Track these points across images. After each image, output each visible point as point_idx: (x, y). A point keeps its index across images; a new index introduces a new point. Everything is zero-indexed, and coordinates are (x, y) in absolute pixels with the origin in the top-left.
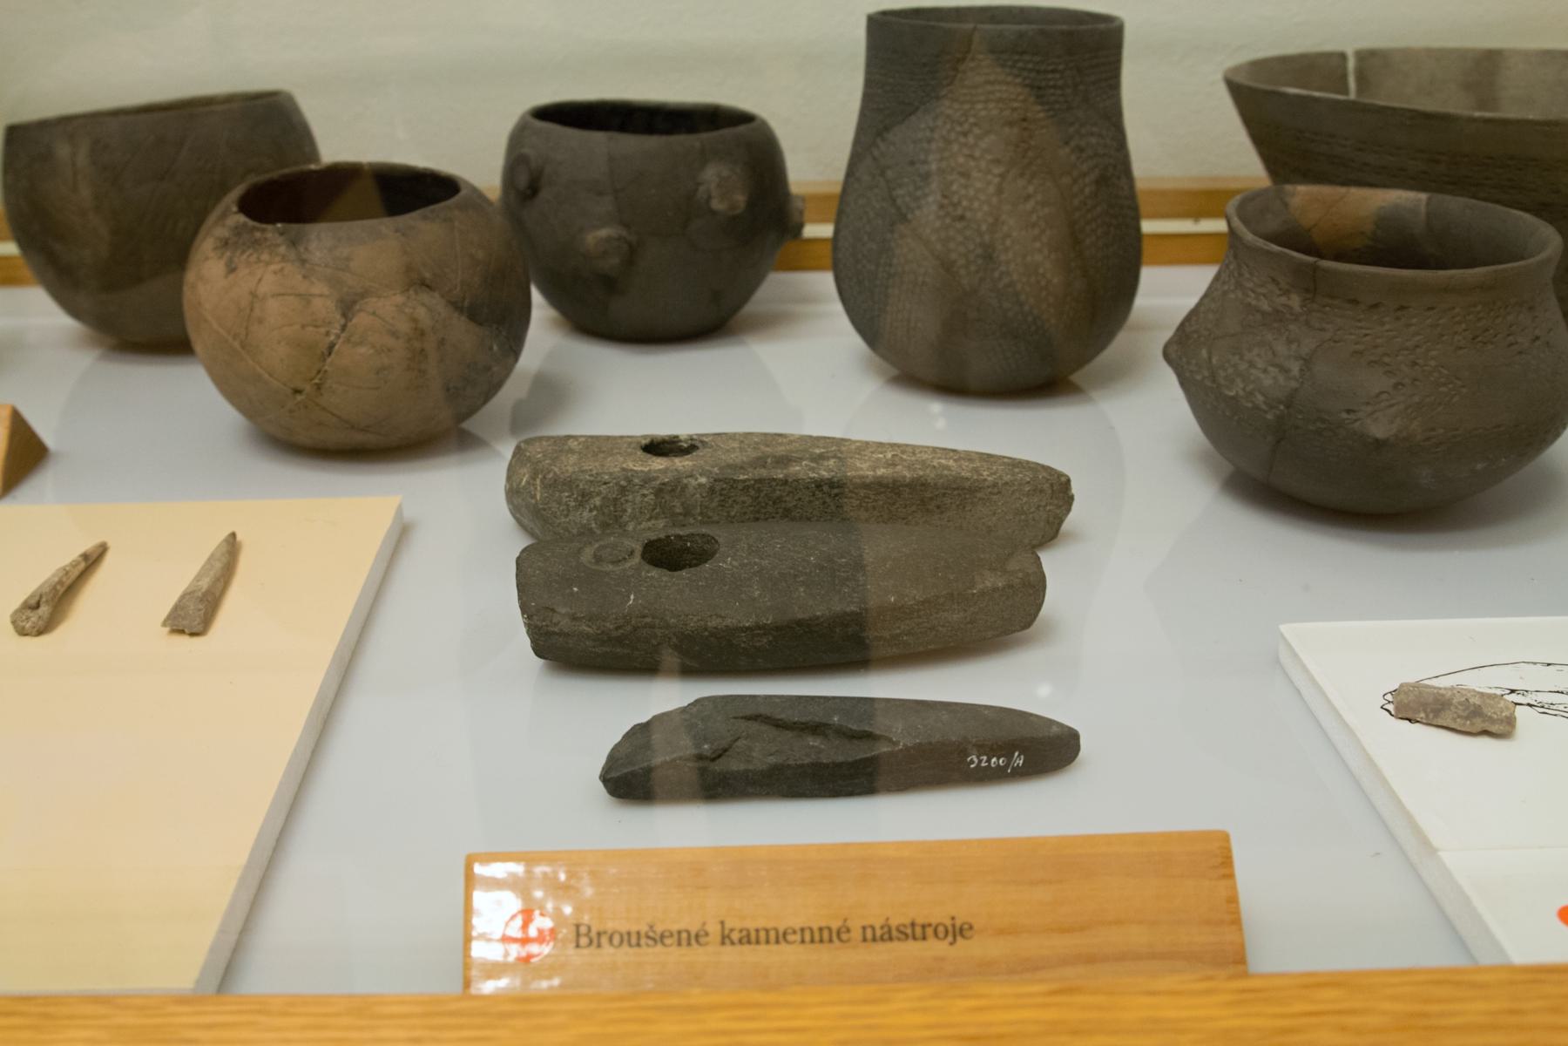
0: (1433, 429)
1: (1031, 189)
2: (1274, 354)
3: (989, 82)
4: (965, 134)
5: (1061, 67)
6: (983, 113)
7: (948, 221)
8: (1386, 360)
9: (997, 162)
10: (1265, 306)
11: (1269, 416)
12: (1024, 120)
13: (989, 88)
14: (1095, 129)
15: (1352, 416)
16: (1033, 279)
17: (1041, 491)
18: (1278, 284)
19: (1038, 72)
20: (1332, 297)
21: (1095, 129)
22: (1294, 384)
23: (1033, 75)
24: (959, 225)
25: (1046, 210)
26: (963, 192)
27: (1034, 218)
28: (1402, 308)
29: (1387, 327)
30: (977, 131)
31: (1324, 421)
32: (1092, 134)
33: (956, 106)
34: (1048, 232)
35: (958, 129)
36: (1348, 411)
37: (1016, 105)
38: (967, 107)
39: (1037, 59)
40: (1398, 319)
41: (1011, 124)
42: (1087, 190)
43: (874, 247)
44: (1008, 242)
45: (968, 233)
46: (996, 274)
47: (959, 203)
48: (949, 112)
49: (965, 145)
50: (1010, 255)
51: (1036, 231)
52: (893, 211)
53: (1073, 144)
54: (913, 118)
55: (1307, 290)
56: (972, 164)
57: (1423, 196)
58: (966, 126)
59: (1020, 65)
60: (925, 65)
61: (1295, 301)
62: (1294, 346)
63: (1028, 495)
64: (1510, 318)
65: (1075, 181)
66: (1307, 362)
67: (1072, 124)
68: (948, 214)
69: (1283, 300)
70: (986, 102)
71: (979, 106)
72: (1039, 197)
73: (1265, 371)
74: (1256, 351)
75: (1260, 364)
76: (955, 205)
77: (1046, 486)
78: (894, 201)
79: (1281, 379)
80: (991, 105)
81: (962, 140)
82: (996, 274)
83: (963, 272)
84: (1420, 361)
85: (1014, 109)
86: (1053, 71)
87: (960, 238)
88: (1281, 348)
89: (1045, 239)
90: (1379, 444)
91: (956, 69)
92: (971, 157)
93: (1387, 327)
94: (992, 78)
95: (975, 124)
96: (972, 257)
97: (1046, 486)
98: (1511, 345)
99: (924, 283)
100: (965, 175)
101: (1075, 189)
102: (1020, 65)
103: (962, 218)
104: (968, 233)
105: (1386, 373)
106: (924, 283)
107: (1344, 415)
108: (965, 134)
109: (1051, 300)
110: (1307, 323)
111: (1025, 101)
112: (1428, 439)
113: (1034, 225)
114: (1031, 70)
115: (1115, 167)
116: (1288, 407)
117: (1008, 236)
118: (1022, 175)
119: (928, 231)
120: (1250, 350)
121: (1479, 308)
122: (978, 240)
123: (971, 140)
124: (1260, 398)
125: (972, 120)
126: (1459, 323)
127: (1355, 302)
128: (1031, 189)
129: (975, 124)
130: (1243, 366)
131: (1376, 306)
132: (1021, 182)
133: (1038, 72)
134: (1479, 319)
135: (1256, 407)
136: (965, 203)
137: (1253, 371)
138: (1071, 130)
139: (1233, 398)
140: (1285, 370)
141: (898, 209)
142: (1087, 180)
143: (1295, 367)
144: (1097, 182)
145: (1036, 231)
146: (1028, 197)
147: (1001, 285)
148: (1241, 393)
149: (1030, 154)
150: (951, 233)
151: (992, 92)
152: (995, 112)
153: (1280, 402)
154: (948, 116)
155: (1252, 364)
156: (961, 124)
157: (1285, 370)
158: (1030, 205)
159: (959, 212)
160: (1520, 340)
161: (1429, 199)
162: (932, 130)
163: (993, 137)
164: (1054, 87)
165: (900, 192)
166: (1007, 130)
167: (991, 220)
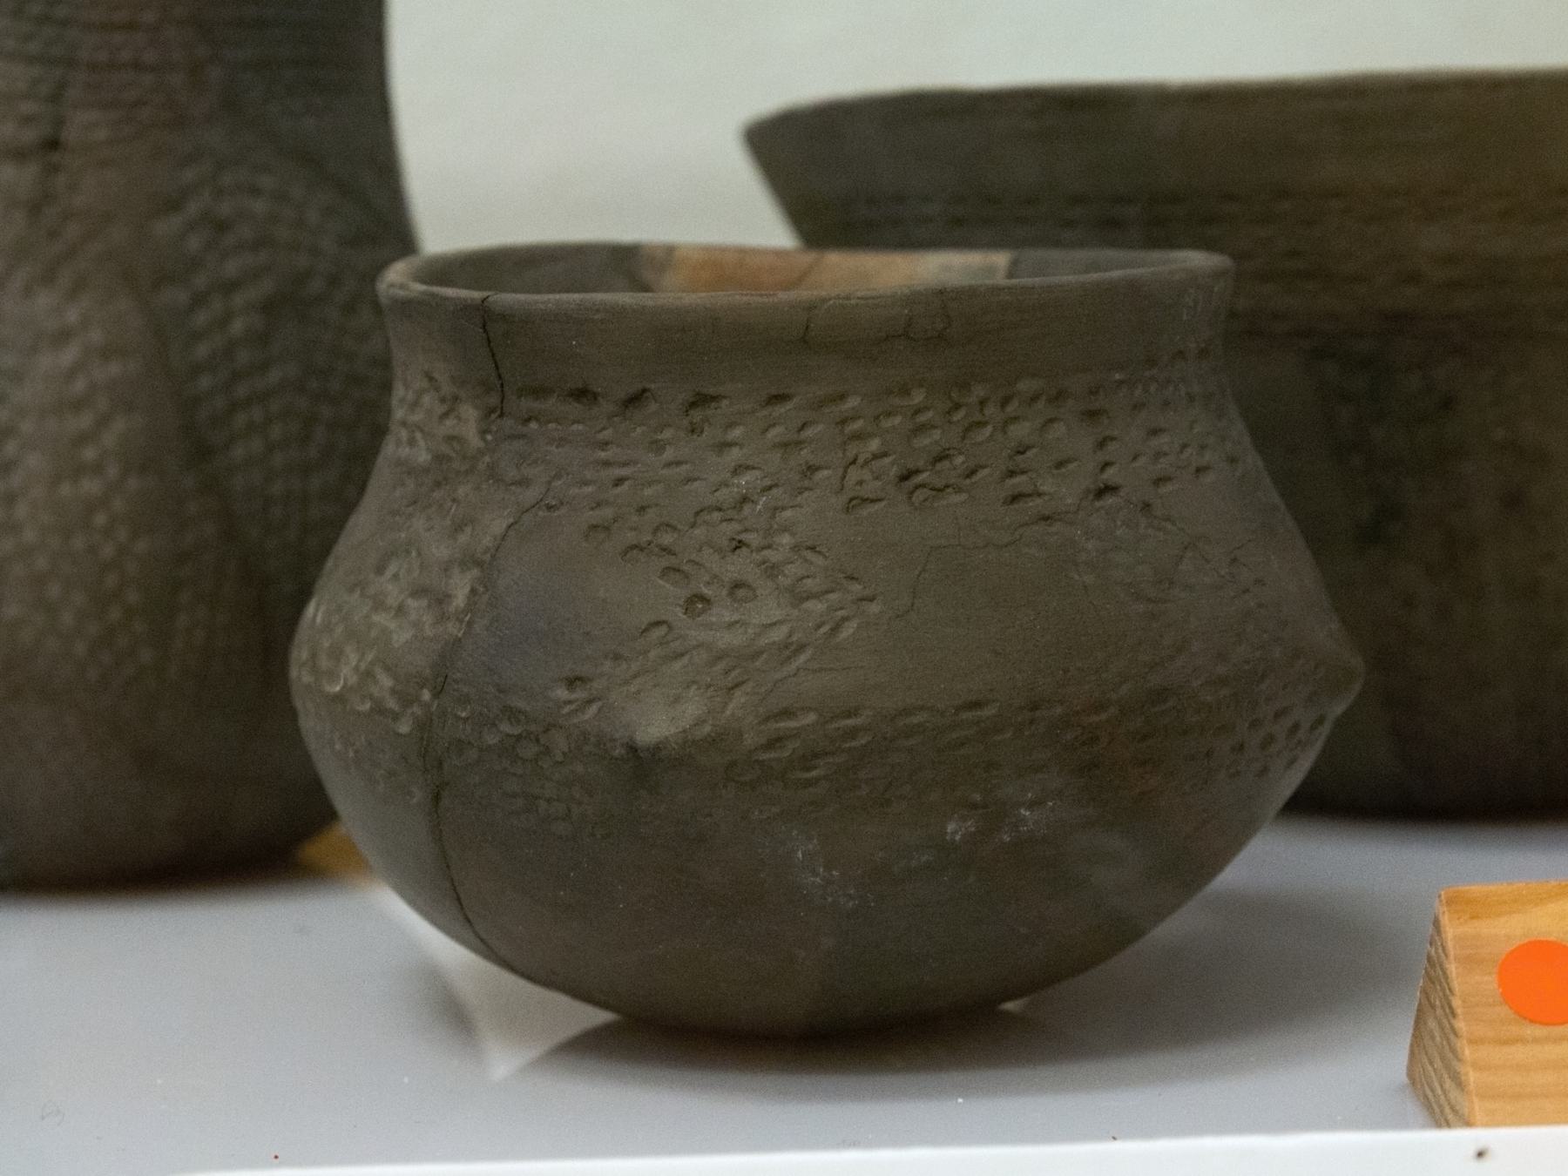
0: (787, 713)
1: (72, 316)
8: (667, 539)
15: (580, 694)
16: (79, 543)
18: (437, 389)
20: (540, 392)
21: (266, 181)
22: (453, 629)
25: (114, 369)
28: (701, 400)
29: (669, 454)
31: (512, 714)
32: (255, 191)
36: (572, 682)
40: (693, 430)
42: (238, 326)
51: (85, 421)
53: (193, 208)
57: (1000, 259)
62: (463, 538)
64: (1020, 431)
65: (199, 300)
66: (485, 565)
72: (96, 336)
73: (401, 610)
84: (753, 538)
90: (643, 765)
93: (669, 454)
98: (1015, 498)
101: (201, 319)
105: (666, 572)
107: (562, 693)
109: (133, 597)
110: (493, 474)
112: (774, 742)
113: (78, 405)
116: (438, 693)
121: (918, 397)
124: (386, 681)
126: (858, 437)
127: (583, 394)
128: (72, 316)
131: (635, 400)
134: (920, 429)
135: (379, 709)
137: (379, 618)
138: (189, 175)
139: (339, 698)
142: (238, 300)
144: (268, 307)
145: (85, 421)
158: (69, 355)
160: (1047, 486)
161: (1015, 263)
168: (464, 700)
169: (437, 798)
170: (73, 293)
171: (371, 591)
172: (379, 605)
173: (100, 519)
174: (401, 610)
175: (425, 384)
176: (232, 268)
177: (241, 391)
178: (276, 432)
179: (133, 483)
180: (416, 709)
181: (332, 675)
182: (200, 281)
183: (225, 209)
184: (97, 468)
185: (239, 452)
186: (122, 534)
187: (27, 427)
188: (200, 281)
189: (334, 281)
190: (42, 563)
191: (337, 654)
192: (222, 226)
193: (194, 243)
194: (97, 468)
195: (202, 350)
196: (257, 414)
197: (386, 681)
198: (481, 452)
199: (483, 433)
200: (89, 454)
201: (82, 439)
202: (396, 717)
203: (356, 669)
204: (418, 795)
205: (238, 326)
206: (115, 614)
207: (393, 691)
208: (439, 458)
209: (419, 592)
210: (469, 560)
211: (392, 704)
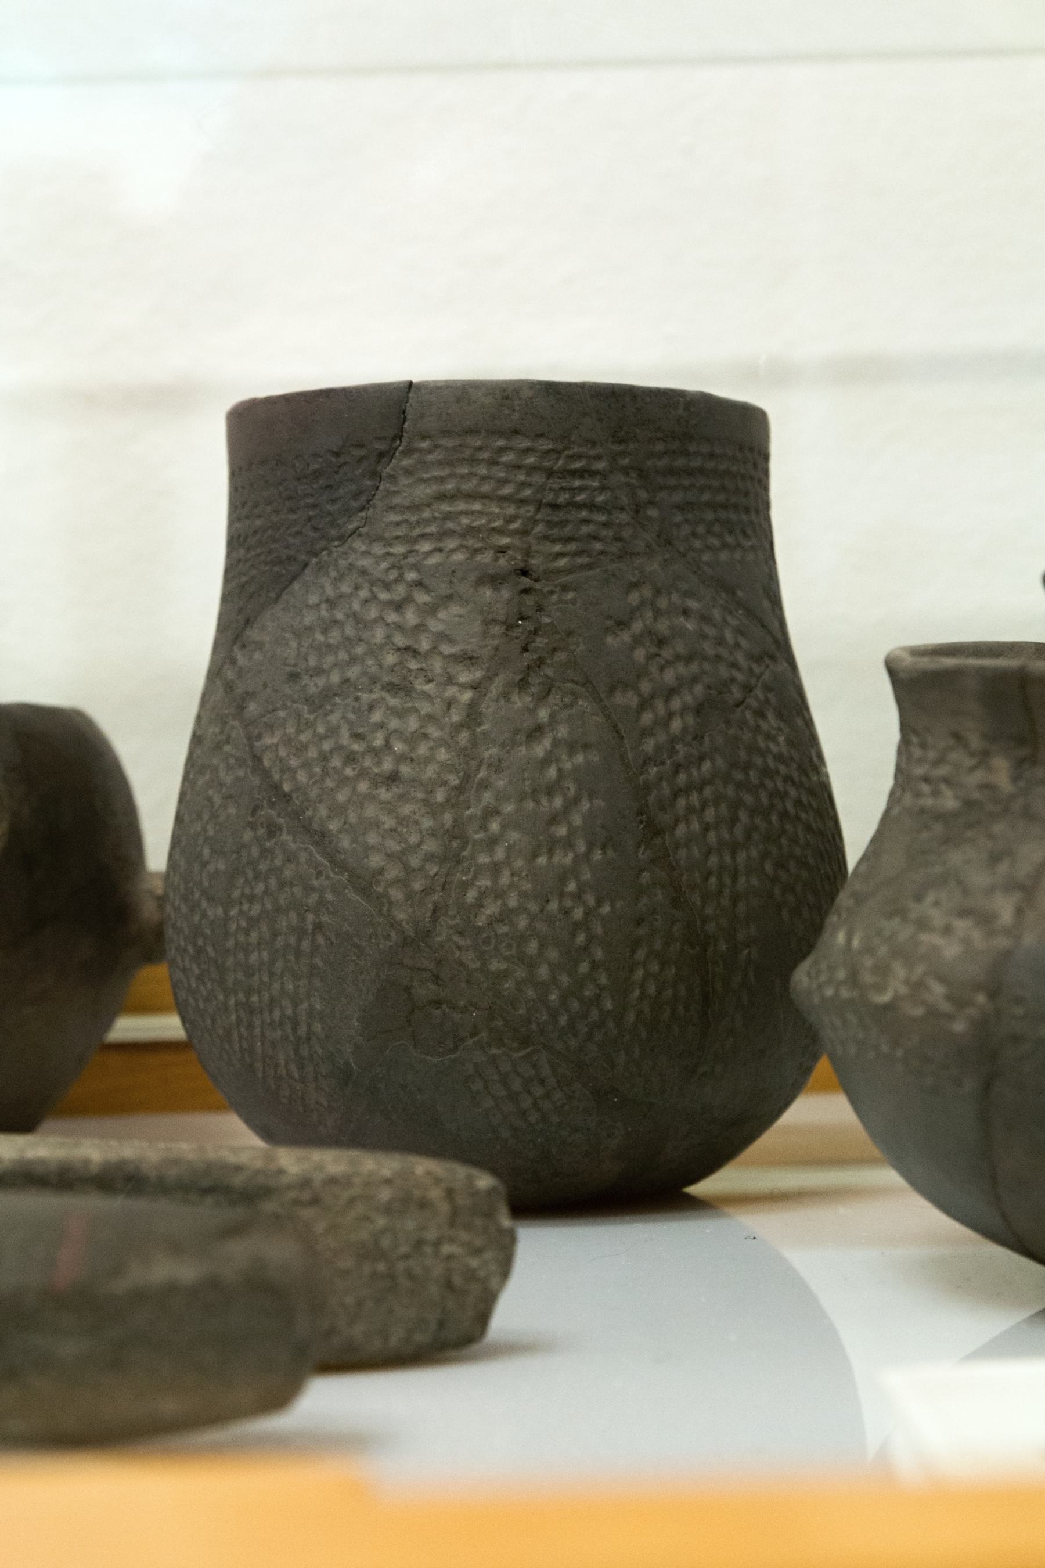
1: (543, 714)
2: (965, 891)
3: (442, 497)
4: (398, 607)
5: (601, 465)
6: (433, 560)
7: (363, 787)
9: (468, 659)
10: (949, 802)
11: (959, 1027)
12: (524, 572)
13: (446, 507)
14: (693, 604)
16: (553, 906)
17: (424, 1204)
18: (966, 746)
19: (550, 473)
21: (693, 604)
22: (1003, 942)
23: (538, 479)
24: (384, 794)
26: (394, 723)
27: (552, 772)
30: (422, 598)
33: (378, 549)
34: (585, 805)
35: (383, 596)
37: (505, 541)
38: (399, 549)
39: (545, 445)
41: (494, 580)
43: (222, 866)
44: (495, 827)
45: (406, 809)
46: (471, 895)
47: (388, 745)
48: (365, 562)
49: (399, 627)
50: (500, 854)
52: (256, 781)
53: (637, 626)
54: (296, 586)
55: (1021, 741)
56: (413, 665)
58: (401, 590)
59: (508, 458)
60: (317, 474)
61: (1001, 772)
62: (1003, 868)
63: (388, 1210)
65: (645, 704)
67: (635, 585)
68: (363, 774)
69: (979, 776)
70: (443, 535)
71: (426, 547)
73: (947, 930)
74: (930, 898)
75: (937, 917)
76: (376, 753)
77: (435, 1194)
78: (257, 759)
79: (977, 935)
80: (451, 544)
81: (392, 617)
82: (471, 895)
83: (397, 894)
85: (502, 551)
86: (581, 473)
87: (389, 822)
88: (979, 879)
89: (577, 820)
91: (376, 475)
92: (411, 651)
94: (450, 486)
95: (419, 584)
96: (415, 862)
97: (435, 1194)
99: (318, 927)
100: (401, 688)
101: (647, 718)
102: (508, 458)
103: (393, 778)
104: (406, 809)
106: (318, 927)
108: (398, 607)
109: (599, 954)
111: (524, 533)
113: (550, 791)
114: (532, 469)
115: (748, 689)
116: (993, 995)
117: (492, 812)
118: (523, 684)
119: (323, 811)
120: (919, 898)
122: (427, 823)
123: (411, 617)
124: (938, 989)
125: (411, 576)
128: (543, 714)
129: (419, 584)
130: (905, 933)
132: (520, 701)
133: (550, 473)
135: (932, 1012)
136: (398, 747)
137: (925, 937)
138: (634, 598)
139: (887, 1007)
140: (986, 920)
141: (266, 774)
142: (676, 704)
143: (1005, 908)
144: (699, 710)
146: (536, 732)
147: (481, 921)
148: (903, 990)
149: (540, 642)
150: (371, 811)
151: (448, 516)
152: (459, 557)
153: (978, 987)
154: (363, 572)
155: (923, 925)
156: (387, 586)
157: (986, 920)
159: (387, 766)
162: (331, 603)
163: (456, 609)
164: (592, 506)
165: (268, 740)
166: (488, 593)
167: (454, 780)
168: (1019, 1001)
169: (987, 1086)
170: (542, 698)
171: (913, 915)
172: (923, 925)
173: (572, 887)
174: (947, 930)
175: (952, 742)
176: (669, 676)
177: (682, 778)
178: (710, 814)
179: (597, 856)
180: (971, 1011)
181: (880, 988)
182: (645, 687)
183: (663, 627)
184: (568, 844)
185: (681, 830)
186: (591, 899)
187: (509, 808)
188: (645, 687)
189: (748, 689)
190: (522, 923)
191: (883, 970)
192: (661, 642)
193: (640, 654)
194: (568, 844)
195: (649, 746)
196: (695, 799)
197: (938, 989)
198: (1012, 797)
199: (1015, 779)
200: (562, 831)
201: (554, 819)
202: (951, 1017)
203: (907, 982)
204: (970, 1085)
205: (676, 725)
206: (584, 968)
207: (948, 997)
208: (969, 804)
209: (964, 913)
210: (1011, 886)
211: (946, 1007)
